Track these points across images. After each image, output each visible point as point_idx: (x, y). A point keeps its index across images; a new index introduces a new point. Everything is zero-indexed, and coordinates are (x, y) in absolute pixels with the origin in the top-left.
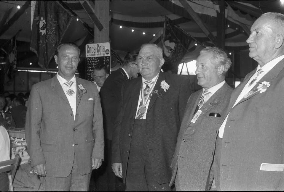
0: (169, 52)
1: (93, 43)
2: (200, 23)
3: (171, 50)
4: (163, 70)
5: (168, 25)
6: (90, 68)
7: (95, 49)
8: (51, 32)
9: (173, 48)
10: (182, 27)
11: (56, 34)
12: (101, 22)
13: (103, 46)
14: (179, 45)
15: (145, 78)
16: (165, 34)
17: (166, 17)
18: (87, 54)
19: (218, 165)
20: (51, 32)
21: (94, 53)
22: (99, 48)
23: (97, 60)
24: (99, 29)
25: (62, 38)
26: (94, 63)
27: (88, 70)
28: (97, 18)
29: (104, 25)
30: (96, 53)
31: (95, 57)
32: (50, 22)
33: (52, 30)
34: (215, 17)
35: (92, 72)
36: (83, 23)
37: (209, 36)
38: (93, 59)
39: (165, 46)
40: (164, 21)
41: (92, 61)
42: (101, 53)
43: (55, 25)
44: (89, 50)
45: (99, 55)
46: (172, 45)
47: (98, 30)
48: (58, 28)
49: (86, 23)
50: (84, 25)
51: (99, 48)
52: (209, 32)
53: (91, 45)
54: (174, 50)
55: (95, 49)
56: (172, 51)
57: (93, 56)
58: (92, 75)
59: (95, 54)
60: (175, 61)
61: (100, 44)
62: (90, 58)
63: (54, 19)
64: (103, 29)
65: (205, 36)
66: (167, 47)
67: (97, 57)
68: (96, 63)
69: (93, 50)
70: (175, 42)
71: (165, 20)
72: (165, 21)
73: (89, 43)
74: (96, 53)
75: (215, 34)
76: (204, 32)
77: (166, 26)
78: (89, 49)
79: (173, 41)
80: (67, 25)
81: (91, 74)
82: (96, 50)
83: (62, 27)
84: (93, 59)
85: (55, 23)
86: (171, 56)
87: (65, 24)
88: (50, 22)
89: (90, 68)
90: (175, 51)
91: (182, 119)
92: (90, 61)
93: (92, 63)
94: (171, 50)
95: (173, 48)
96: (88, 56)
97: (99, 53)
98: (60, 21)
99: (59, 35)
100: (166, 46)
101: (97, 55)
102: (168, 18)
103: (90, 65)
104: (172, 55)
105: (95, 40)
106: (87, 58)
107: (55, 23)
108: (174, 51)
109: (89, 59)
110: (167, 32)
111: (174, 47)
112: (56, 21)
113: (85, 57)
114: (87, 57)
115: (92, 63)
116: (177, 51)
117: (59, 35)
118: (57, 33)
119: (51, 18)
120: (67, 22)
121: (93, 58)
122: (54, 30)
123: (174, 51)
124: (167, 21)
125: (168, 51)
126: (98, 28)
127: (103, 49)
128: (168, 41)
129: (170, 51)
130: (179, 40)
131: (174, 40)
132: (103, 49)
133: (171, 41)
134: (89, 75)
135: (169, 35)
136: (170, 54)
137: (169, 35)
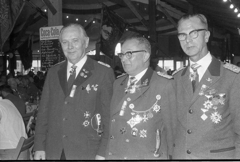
0: (107, 36)
1: (47, 26)
2: (134, 10)
3: (108, 33)
4: (103, 52)
5: (105, 11)
6: (45, 50)
7: (49, 32)
8: (4, 16)
9: (110, 32)
10: (118, 13)
11: (8, 18)
12: (54, 7)
13: (57, 29)
14: (116, 28)
15: (72, 62)
16: (103, 20)
17: (103, 4)
18: (41, 37)
19: (177, 108)
20: (4, 16)
21: (48, 36)
22: (53, 31)
23: (52, 43)
24: (53, 13)
25: (15, 22)
26: (49, 45)
27: (42, 52)
28: (50, 3)
29: (57, 10)
30: (51, 36)
31: (49, 40)
32: (3, 7)
33: (5, 14)
34: (147, 4)
35: (47, 54)
36: (36, 7)
37: (142, 20)
38: (47, 41)
39: (103, 30)
40: (102, 8)
41: (46, 43)
42: (55, 36)
43: (7, 9)
44: (43, 33)
45: (53, 37)
46: (110, 29)
47: (52, 14)
48: (11, 12)
49: (38, 8)
50: (37, 9)
51: (53, 31)
52: (142, 17)
53: (45, 29)
54: (111, 33)
55: (49, 32)
56: (109, 34)
57: (47, 39)
58: (47, 57)
59: (49, 36)
60: (112, 43)
61: (54, 28)
62: (44, 41)
63: (6, 4)
64: (57, 13)
65: (138, 21)
66: (105, 31)
67: (51, 40)
68: (51, 45)
69: (47, 33)
70: (111, 26)
71: (103, 6)
72: (102, 8)
73: (43, 26)
74: (51, 36)
75: (147, 18)
76: (137, 18)
77: (104, 12)
78: (43, 33)
79: (110, 26)
80: (19, 9)
81: (46, 56)
82: (50, 33)
83: (14, 11)
84: (47, 41)
85: (8, 8)
86: (108, 39)
87: (17, 9)
88: (3, 7)
89: (45, 50)
90: (112, 34)
91: (211, 55)
92: (44, 43)
93: (47, 45)
94: (108, 34)
95: (110, 32)
96: (42, 38)
97: (53, 36)
98: (12, 6)
99: (12, 19)
100: (104, 30)
101: (51, 37)
102: (105, 5)
103: (44, 47)
104: (110, 38)
105: (49, 24)
106: (41, 41)
107: (8, 8)
108: (111, 35)
109: (44, 42)
110: (105, 17)
111: (111, 31)
112: (8, 6)
113: (39, 40)
114: (41, 39)
115: (47, 45)
116: (113, 34)
117: (12, 19)
118: (10, 17)
119: (3, 3)
120: (19, 7)
121: (47, 40)
122: (6, 14)
123: (111, 35)
124: (104, 8)
125: (105, 34)
126: (52, 12)
127: (57, 31)
128: (106, 26)
129: (107, 35)
130: (115, 25)
131: (111, 24)
132: (57, 31)
133: (108, 25)
134: (43, 57)
135: (107, 20)
136: (107, 37)
137: (107, 20)
